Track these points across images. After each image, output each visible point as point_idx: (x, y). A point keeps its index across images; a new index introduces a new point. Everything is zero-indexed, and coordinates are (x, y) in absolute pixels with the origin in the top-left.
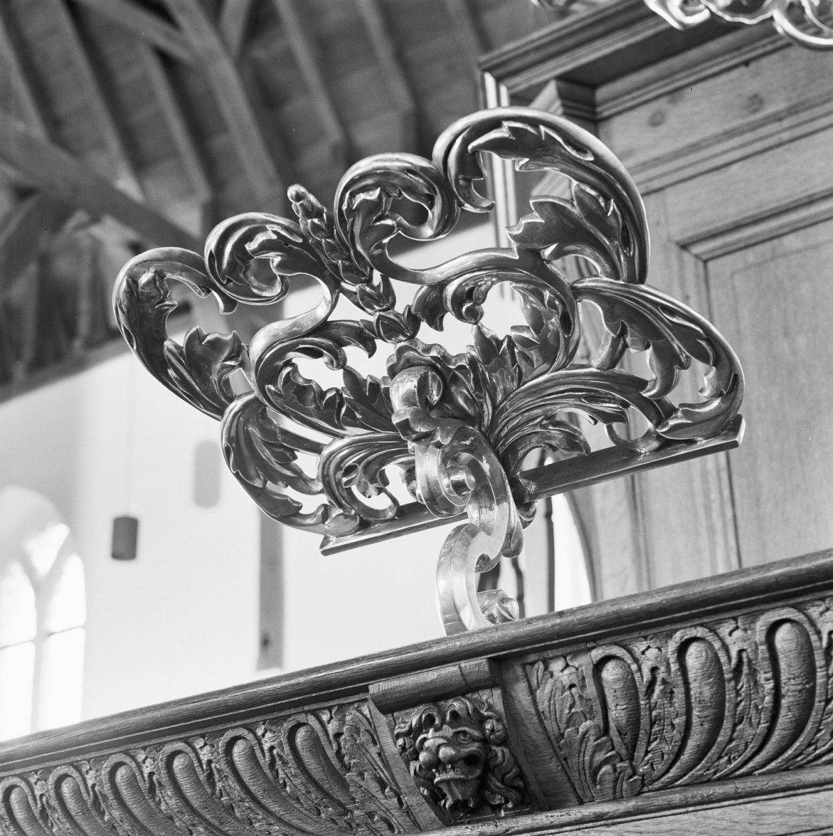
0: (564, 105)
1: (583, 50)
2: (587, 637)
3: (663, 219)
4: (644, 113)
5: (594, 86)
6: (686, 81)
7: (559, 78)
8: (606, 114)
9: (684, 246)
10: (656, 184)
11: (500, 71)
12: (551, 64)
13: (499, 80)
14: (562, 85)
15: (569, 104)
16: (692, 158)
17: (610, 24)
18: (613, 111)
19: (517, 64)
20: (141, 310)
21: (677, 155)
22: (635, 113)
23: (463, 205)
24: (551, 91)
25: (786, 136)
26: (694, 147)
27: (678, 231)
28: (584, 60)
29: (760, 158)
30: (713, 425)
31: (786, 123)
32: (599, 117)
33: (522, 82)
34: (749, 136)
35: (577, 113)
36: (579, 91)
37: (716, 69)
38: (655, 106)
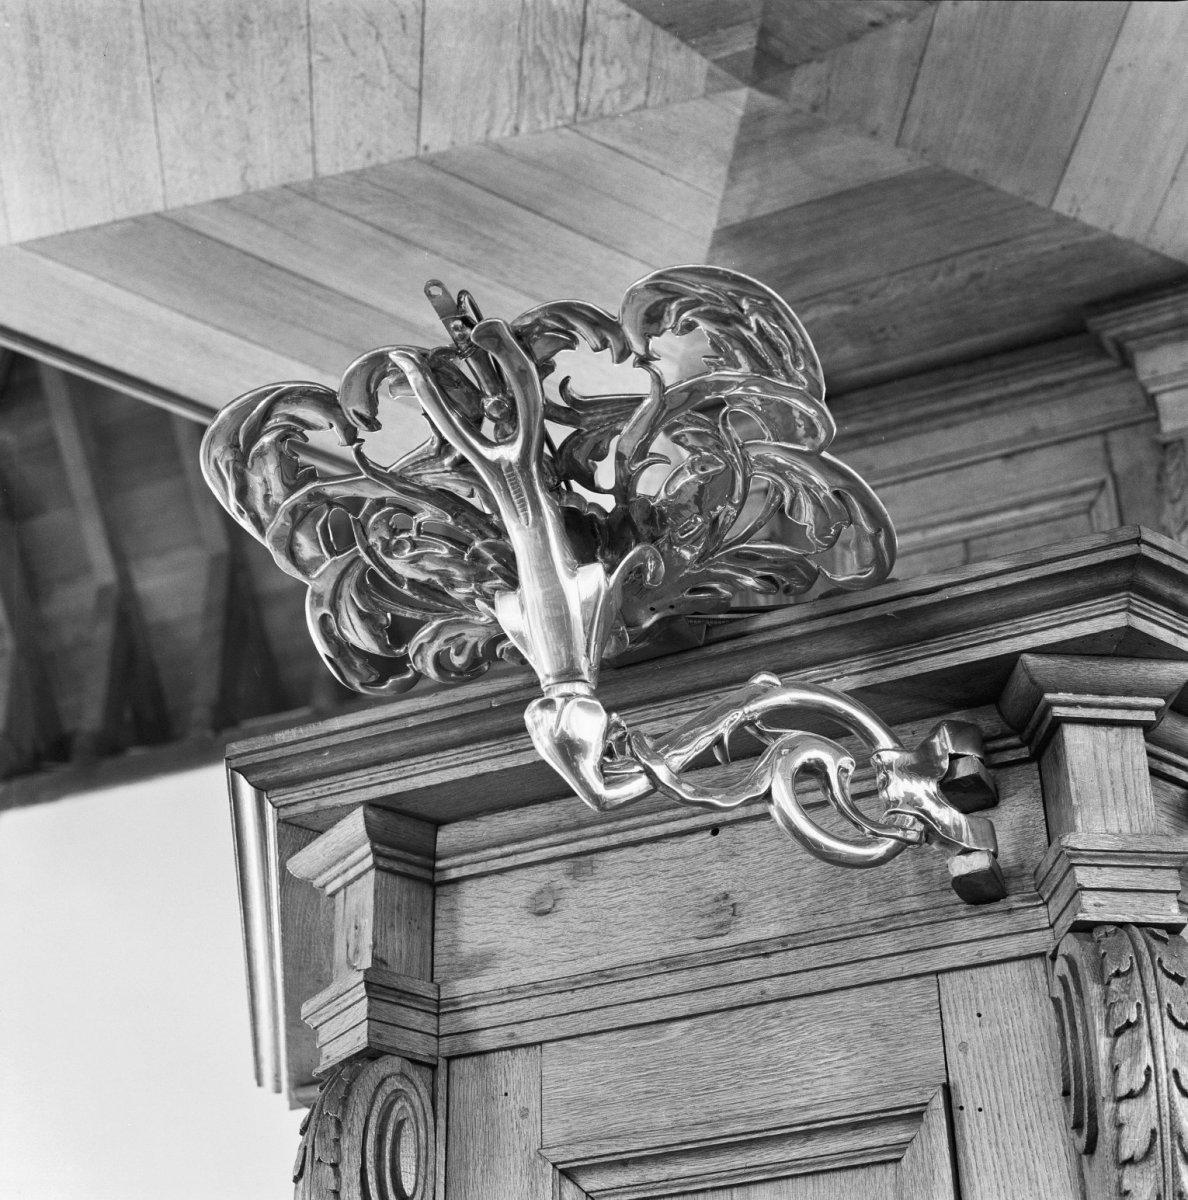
0: (376, 854)
1: (423, 763)
2: (776, 292)
3: (534, 1105)
4: (523, 886)
5: (438, 824)
6: (603, 842)
7: (370, 805)
8: (454, 874)
9: (568, 1173)
10: (528, 1033)
11: (268, 776)
12: (361, 777)
13: (261, 789)
14: (371, 814)
15: (387, 850)
16: (600, 995)
17: (473, 728)
18: (465, 871)
19: (297, 769)
20: (432, 454)
21: (574, 984)
22: (503, 882)
23: (601, 457)
24: (353, 827)
25: (772, 988)
26: (604, 977)
27: (560, 1133)
28: (421, 782)
29: (723, 1022)
30: (781, 322)
31: (776, 963)
32: (438, 877)
33: (304, 800)
34: (706, 975)
35: (396, 866)
36: (407, 830)
37: (659, 830)
38: (542, 875)
